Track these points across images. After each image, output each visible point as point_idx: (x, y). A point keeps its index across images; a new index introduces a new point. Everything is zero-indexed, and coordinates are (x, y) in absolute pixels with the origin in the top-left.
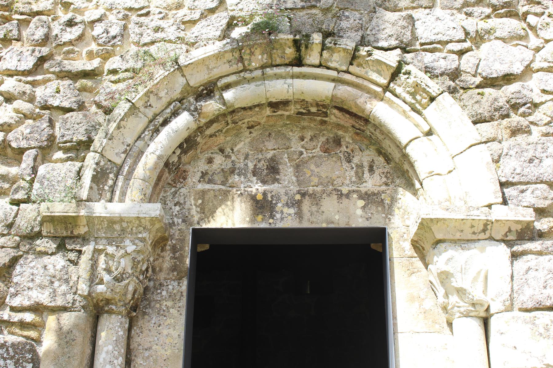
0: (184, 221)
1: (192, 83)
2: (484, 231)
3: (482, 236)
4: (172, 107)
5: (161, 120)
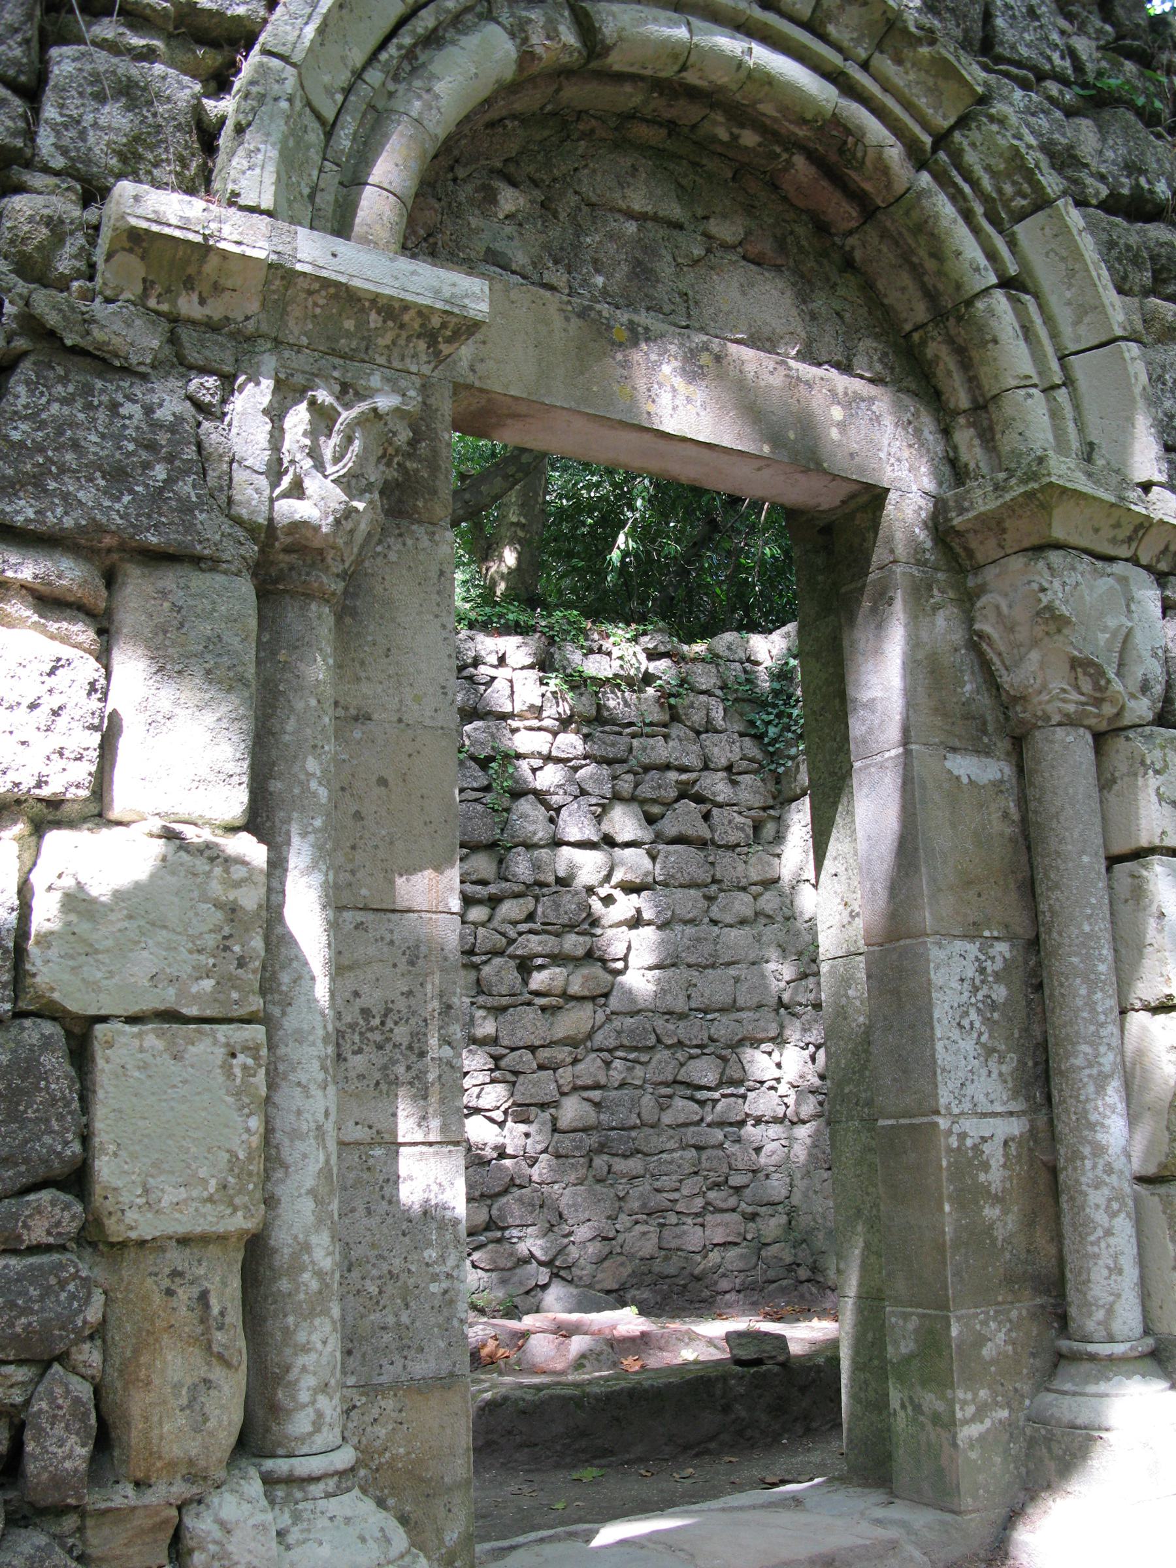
3: (1124, 552)
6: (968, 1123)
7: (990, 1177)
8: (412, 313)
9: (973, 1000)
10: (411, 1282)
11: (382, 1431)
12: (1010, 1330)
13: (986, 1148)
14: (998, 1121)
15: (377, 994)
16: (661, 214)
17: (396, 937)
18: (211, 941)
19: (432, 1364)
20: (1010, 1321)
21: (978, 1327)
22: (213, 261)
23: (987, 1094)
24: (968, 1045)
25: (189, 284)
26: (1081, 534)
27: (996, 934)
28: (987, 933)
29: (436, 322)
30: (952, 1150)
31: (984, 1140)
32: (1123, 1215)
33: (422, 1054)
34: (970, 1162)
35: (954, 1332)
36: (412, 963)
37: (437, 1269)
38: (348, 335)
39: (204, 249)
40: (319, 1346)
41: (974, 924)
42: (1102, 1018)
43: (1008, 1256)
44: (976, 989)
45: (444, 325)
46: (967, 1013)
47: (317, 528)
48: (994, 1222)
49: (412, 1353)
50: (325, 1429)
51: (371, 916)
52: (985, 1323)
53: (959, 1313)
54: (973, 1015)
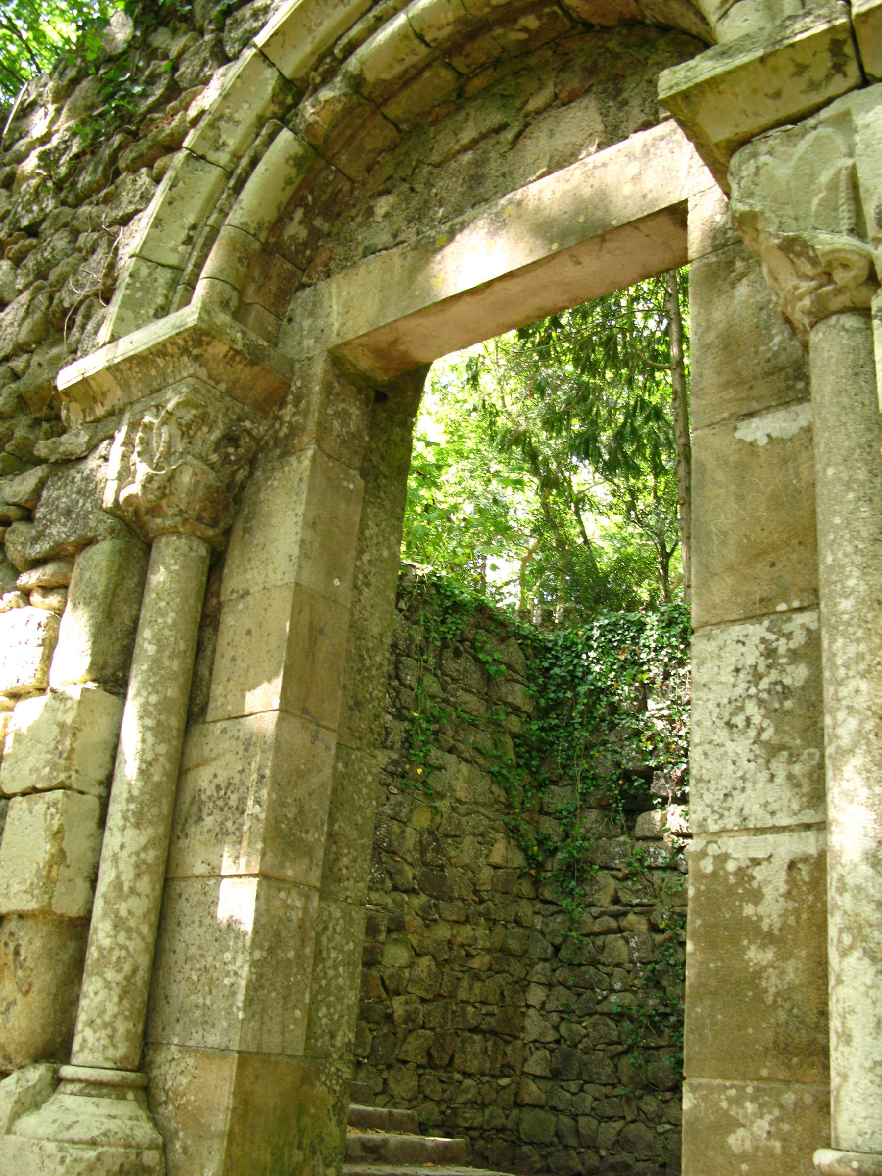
0: (317, 339)
1: (287, 73)
2: (838, 68)
3: (839, 84)
4: (264, 132)
5: (245, 161)
6: (731, 842)
7: (761, 909)
8: (169, 346)
9: (753, 691)
10: (215, 975)
11: (184, 1080)
12: (779, 1119)
13: (759, 873)
14: (784, 837)
15: (226, 774)
16: (484, 131)
17: (241, 734)
18: (52, 746)
19: (218, 1039)
20: (781, 1107)
21: (724, 1105)
22: (92, 382)
23: (766, 804)
24: (741, 747)
25: (95, 400)
26: (756, 114)
27: (796, 604)
28: (782, 607)
29: (181, 342)
30: (705, 876)
31: (756, 862)
32: (857, 953)
33: (243, 812)
34: (730, 891)
35: (686, 1104)
36: (246, 750)
37: (230, 967)
38: (155, 378)
39: (85, 381)
40: (92, 995)
41: (762, 600)
42: (842, 672)
43: (782, 1016)
44: (757, 677)
45: (185, 341)
46: (742, 709)
47: (136, 496)
48: (764, 968)
49: (207, 1027)
50: (86, 1051)
51: (230, 722)
52: (737, 1101)
53: (696, 1081)
54: (751, 708)
